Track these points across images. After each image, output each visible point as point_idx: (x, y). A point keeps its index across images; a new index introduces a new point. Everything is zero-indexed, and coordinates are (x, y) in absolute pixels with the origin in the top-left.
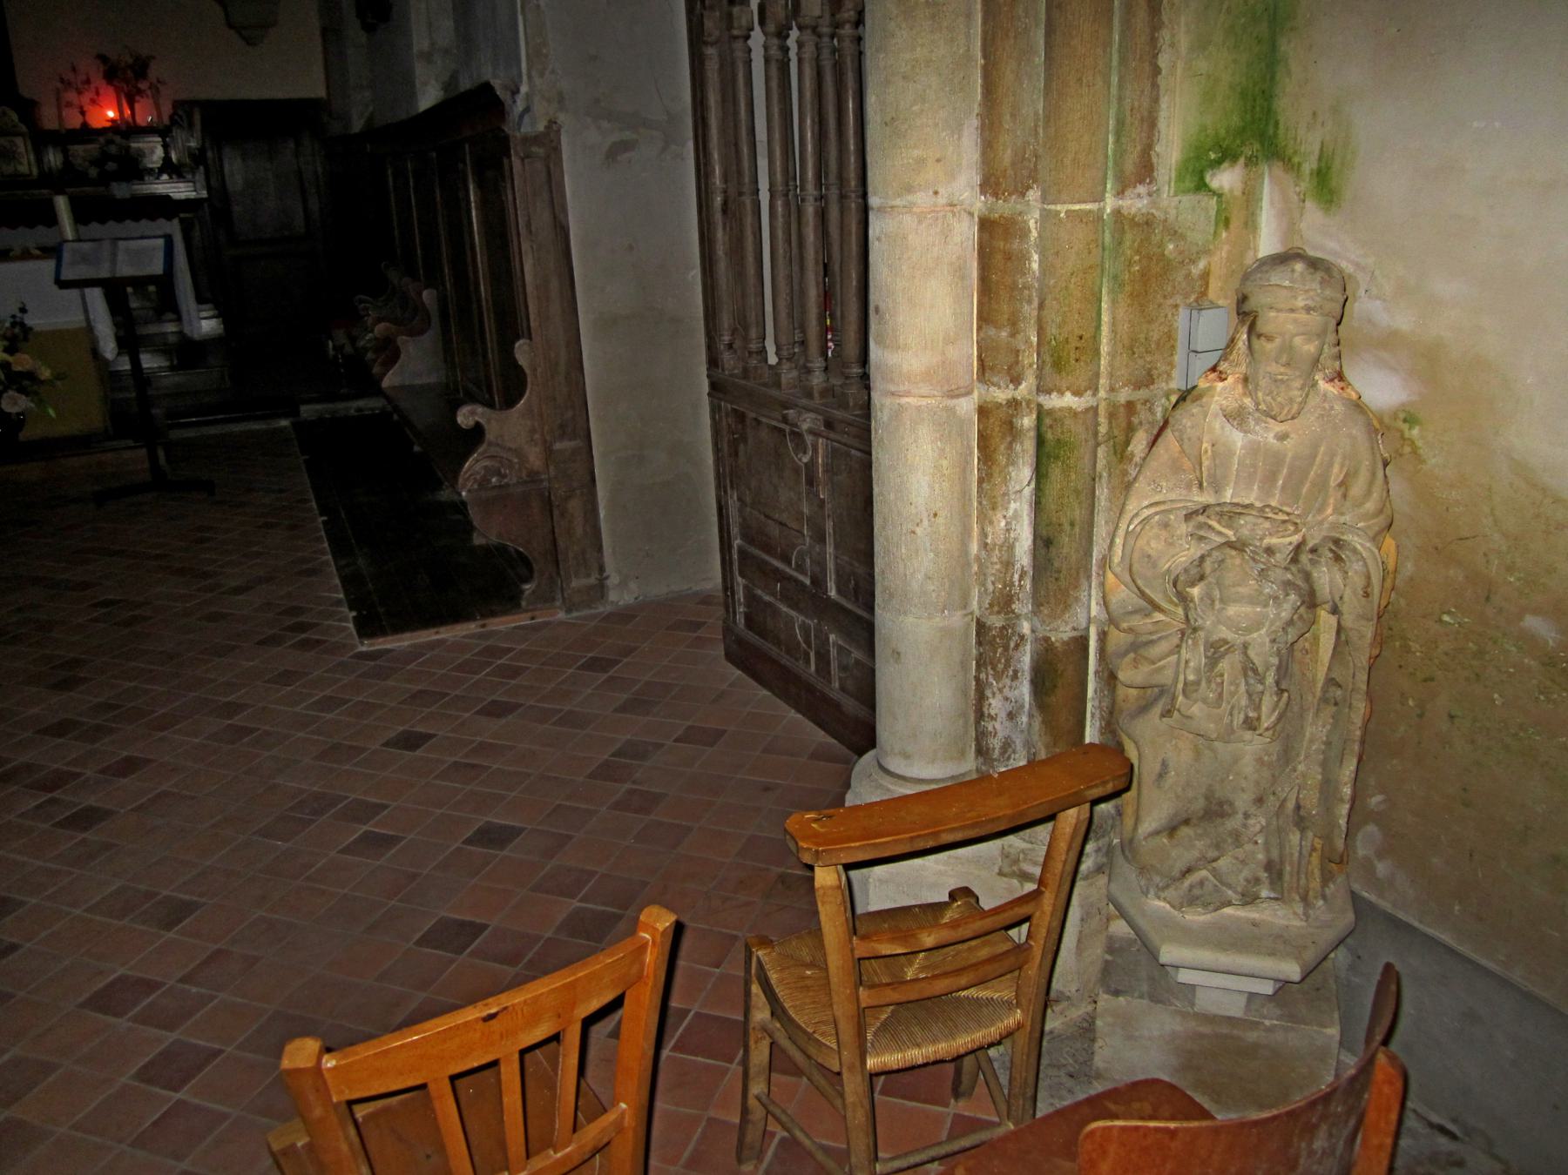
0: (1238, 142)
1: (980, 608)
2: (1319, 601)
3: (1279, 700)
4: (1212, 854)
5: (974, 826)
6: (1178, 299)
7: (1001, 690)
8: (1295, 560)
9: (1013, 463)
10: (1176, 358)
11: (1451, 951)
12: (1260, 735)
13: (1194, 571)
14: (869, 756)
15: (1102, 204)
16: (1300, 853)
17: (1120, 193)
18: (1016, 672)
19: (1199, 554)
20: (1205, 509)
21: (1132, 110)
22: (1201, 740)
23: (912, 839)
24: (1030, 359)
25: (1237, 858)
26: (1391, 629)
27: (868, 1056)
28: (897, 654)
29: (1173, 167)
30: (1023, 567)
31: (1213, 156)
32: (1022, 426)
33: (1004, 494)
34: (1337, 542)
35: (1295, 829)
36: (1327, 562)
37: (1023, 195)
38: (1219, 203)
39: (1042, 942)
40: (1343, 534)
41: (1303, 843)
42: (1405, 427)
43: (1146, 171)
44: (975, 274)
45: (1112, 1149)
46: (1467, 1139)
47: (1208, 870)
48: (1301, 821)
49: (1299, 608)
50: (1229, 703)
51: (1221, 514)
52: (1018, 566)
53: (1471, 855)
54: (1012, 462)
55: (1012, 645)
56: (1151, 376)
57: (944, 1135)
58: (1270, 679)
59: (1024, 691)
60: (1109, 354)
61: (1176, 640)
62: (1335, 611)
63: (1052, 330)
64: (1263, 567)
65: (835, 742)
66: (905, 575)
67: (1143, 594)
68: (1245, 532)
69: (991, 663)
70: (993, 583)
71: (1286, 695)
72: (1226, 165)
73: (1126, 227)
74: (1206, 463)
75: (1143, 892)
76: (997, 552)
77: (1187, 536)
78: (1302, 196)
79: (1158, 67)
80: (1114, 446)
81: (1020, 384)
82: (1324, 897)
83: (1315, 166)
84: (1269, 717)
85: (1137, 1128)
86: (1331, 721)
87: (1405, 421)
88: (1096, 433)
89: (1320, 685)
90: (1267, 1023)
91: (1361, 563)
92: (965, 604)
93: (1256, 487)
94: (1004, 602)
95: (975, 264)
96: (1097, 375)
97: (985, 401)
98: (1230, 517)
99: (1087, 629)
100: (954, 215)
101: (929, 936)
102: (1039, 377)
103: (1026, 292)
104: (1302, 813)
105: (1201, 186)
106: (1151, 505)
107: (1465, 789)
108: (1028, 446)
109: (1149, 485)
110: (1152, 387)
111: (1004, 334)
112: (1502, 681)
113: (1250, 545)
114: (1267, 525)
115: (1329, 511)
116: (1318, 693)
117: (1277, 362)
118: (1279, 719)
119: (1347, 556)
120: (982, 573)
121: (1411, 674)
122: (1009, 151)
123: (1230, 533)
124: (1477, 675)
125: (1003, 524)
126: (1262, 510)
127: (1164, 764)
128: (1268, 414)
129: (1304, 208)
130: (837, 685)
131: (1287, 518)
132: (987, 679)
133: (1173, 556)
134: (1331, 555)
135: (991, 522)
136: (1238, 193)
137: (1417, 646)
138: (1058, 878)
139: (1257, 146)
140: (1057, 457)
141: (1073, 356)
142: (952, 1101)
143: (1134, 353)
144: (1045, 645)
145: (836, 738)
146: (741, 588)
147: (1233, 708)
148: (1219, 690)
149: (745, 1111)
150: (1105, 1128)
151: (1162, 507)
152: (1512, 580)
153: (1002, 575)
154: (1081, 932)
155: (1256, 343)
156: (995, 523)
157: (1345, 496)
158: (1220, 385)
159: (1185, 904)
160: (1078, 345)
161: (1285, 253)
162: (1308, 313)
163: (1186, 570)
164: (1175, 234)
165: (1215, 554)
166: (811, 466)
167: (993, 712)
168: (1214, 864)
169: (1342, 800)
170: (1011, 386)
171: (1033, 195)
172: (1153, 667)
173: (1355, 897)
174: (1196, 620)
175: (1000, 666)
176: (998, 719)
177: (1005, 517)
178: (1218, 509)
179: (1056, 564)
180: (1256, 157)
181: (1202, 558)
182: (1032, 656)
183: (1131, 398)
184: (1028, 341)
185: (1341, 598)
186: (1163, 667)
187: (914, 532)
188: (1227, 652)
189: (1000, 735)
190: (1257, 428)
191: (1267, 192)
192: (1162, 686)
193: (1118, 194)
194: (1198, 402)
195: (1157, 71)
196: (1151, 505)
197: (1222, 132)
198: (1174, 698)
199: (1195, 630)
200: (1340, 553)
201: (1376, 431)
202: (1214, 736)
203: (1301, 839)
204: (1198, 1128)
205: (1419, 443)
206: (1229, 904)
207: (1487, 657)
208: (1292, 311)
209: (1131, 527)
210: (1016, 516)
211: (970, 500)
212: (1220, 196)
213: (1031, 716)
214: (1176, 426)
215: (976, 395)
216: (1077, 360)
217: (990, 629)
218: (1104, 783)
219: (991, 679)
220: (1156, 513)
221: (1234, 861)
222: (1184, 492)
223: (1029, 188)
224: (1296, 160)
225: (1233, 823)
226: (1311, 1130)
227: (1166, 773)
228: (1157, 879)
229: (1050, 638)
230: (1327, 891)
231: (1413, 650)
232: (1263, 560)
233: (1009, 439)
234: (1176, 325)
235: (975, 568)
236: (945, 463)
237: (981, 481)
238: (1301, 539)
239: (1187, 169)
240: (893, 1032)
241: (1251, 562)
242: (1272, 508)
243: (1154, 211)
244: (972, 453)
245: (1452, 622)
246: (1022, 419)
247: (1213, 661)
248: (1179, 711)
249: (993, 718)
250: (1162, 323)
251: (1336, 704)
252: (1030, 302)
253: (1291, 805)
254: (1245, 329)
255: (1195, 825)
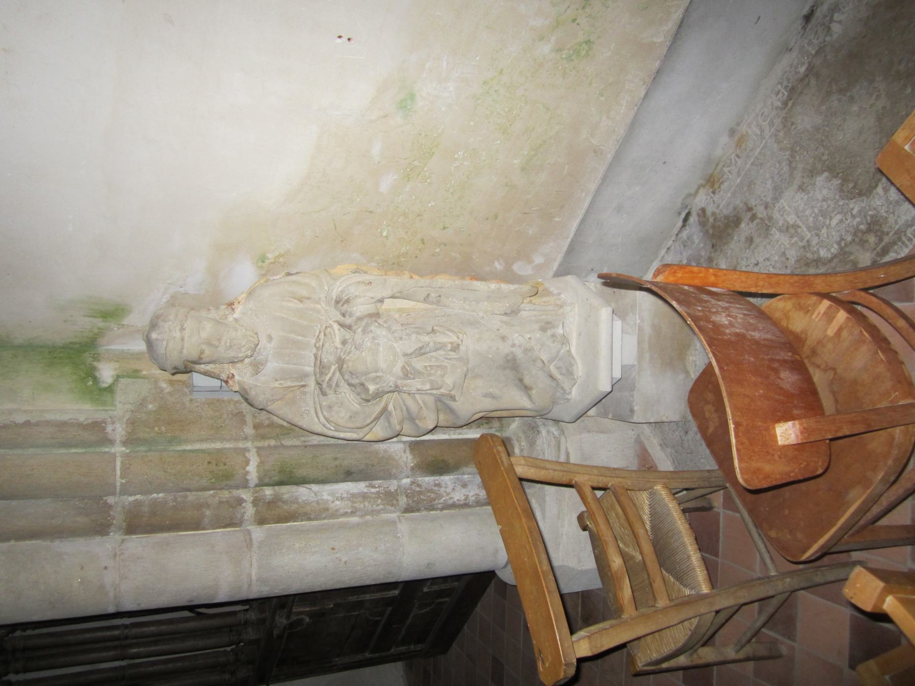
0: (82, 367)
1: (394, 512)
2: (375, 311)
3: (440, 332)
4: (539, 364)
5: (536, 547)
6: (186, 400)
7: (448, 494)
8: (349, 327)
9: (297, 499)
10: (226, 398)
11: (583, 221)
12: (462, 341)
13: (359, 389)
14: (497, 572)
15: (117, 455)
16: (534, 310)
17: (111, 442)
18: (436, 485)
19: (347, 387)
20: (318, 384)
21: (53, 439)
22: (469, 375)
23: (549, 592)
24: (225, 495)
25: (540, 349)
26: (394, 264)
27: (701, 592)
28: (429, 565)
29: (96, 408)
30: (366, 486)
31: (90, 383)
32: (271, 495)
33: (318, 503)
34: (337, 302)
35: (519, 315)
36: (350, 307)
37: (110, 507)
38: (123, 377)
39: (608, 478)
40: (332, 298)
41: (527, 309)
42: (267, 262)
43: (97, 426)
44: (166, 535)
45: (755, 465)
46: (689, 207)
47: (550, 365)
48: (514, 312)
49: (379, 324)
50: (443, 361)
51: (322, 373)
52: (366, 490)
53: (526, 213)
54: (295, 501)
55: (418, 489)
56: (237, 414)
57: (738, 515)
58: (426, 339)
59: (447, 479)
60: (222, 442)
61: (405, 396)
62: (381, 301)
63: (204, 482)
64: (354, 347)
65: (493, 582)
66: (375, 565)
67: (377, 418)
68: (332, 358)
69: (431, 502)
70: (378, 505)
71: (435, 328)
72: (97, 374)
73: (135, 437)
74: (289, 384)
75: (568, 402)
76: (357, 505)
77: (337, 394)
78: (120, 326)
79: (25, 422)
80: (283, 435)
81: (242, 499)
82: (559, 294)
83: (101, 319)
84: (450, 336)
85: (738, 450)
86: (451, 299)
87: (263, 262)
88: (275, 447)
89: (429, 306)
90: (638, 321)
91: (350, 288)
92: (393, 523)
93: (303, 353)
94: (390, 497)
95: (159, 535)
96: (236, 450)
97: (254, 521)
98: (323, 368)
99: (404, 442)
100: (122, 554)
101: (615, 562)
102: (237, 487)
103: (179, 499)
104: (508, 312)
105: (110, 389)
106: (317, 417)
107: (487, 219)
108: (284, 489)
109: (304, 418)
110: (245, 413)
111: (208, 513)
112: (420, 202)
113: (340, 355)
114: (327, 345)
115: (318, 306)
116: (434, 307)
117: (217, 347)
118: (451, 331)
119: (346, 296)
120: (373, 513)
121: (420, 251)
122: (78, 519)
123: (333, 368)
124: (418, 216)
125: (338, 503)
126: (318, 348)
127: (486, 395)
128: (254, 350)
129: (128, 325)
130: (456, 583)
131: (323, 333)
132: (441, 503)
133: (349, 401)
134: (346, 306)
135: (337, 510)
136: (117, 365)
137: (404, 248)
138: (565, 473)
139: (87, 355)
140: (291, 472)
141: (222, 467)
142: (715, 510)
143: (221, 426)
144: (416, 469)
145: (490, 582)
146: (398, 649)
147: (446, 359)
148: (435, 368)
149: (747, 659)
150: (742, 473)
151: (318, 409)
152: (359, 200)
153: (372, 500)
154: (597, 432)
155: (206, 359)
156: (337, 507)
157: (309, 298)
158: (237, 378)
159: (573, 377)
160: (214, 464)
161: (146, 342)
162: (185, 329)
163: (358, 394)
164: (143, 403)
165: (346, 377)
166: (310, 615)
167: (463, 498)
168: (546, 362)
169: (499, 289)
170: (244, 505)
171: (111, 500)
172: (424, 408)
173: (558, 274)
174: (391, 387)
175: (433, 495)
176: (467, 493)
177: (333, 502)
178: (318, 376)
179: (362, 467)
180: (94, 354)
181: (350, 385)
182: (425, 477)
183: (252, 426)
184: (213, 496)
185: (372, 298)
186: (424, 402)
187: (345, 563)
188: (409, 365)
189: (477, 491)
190: (264, 354)
191: (116, 347)
192: (436, 400)
193: (112, 443)
194: (248, 391)
195: (27, 423)
196: (317, 417)
197: (74, 377)
198: (442, 395)
199: (397, 386)
200: (344, 300)
201: (267, 281)
202: (465, 369)
203: (525, 310)
204: (730, 407)
205: (277, 254)
206: (569, 351)
207: (407, 211)
208: (183, 339)
209: (332, 428)
210: (332, 494)
211: (322, 525)
212: (118, 377)
213: (463, 474)
214: (264, 404)
215: (250, 527)
216: (225, 464)
217: (409, 504)
218: (498, 452)
219: (442, 501)
220: (322, 413)
221: (542, 350)
222: (308, 395)
223: (106, 503)
224: (96, 331)
225: (519, 353)
226: (717, 327)
227: (491, 394)
228: (558, 394)
229: (412, 467)
230: (555, 292)
231: (405, 251)
232: (350, 347)
233: (280, 503)
234: (203, 400)
235: (368, 517)
236: (297, 545)
237: (309, 519)
238: (336, 323)
239: (97, 399)
240: (682, 576)
241: (351, 355)
242: (317, 342)
243: (125, 420)
244: (290, 527)
245: (387, 231)
246: (267, 495)
247: (417, 373)
248: (450, 391)
249: (467, 497)
250: (202, 410)
251: (440, 296)
252: (186, 497)
253: (505, 318)
254: (197, 367)
255: (523, 375)
